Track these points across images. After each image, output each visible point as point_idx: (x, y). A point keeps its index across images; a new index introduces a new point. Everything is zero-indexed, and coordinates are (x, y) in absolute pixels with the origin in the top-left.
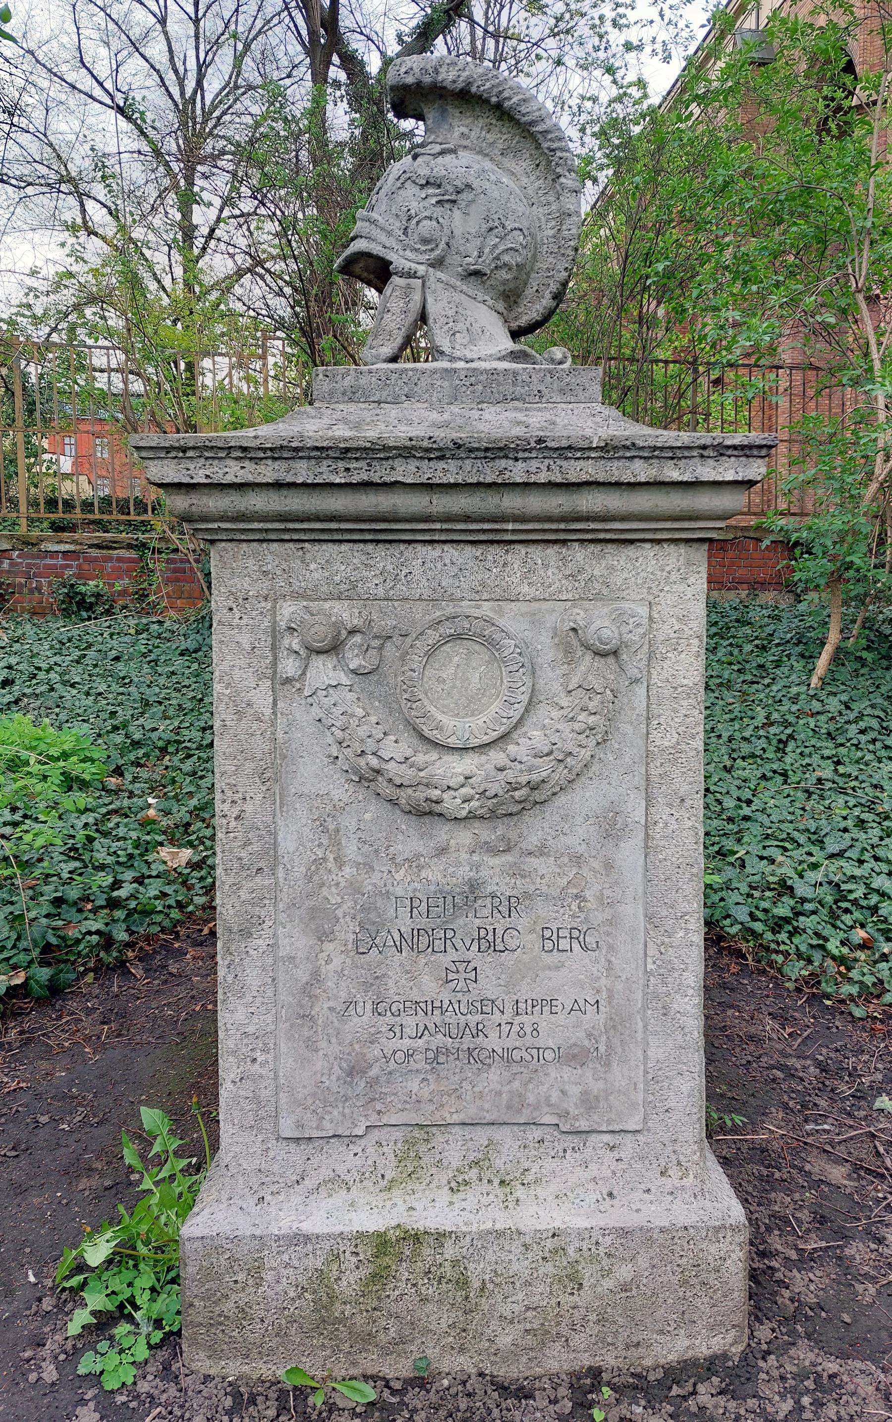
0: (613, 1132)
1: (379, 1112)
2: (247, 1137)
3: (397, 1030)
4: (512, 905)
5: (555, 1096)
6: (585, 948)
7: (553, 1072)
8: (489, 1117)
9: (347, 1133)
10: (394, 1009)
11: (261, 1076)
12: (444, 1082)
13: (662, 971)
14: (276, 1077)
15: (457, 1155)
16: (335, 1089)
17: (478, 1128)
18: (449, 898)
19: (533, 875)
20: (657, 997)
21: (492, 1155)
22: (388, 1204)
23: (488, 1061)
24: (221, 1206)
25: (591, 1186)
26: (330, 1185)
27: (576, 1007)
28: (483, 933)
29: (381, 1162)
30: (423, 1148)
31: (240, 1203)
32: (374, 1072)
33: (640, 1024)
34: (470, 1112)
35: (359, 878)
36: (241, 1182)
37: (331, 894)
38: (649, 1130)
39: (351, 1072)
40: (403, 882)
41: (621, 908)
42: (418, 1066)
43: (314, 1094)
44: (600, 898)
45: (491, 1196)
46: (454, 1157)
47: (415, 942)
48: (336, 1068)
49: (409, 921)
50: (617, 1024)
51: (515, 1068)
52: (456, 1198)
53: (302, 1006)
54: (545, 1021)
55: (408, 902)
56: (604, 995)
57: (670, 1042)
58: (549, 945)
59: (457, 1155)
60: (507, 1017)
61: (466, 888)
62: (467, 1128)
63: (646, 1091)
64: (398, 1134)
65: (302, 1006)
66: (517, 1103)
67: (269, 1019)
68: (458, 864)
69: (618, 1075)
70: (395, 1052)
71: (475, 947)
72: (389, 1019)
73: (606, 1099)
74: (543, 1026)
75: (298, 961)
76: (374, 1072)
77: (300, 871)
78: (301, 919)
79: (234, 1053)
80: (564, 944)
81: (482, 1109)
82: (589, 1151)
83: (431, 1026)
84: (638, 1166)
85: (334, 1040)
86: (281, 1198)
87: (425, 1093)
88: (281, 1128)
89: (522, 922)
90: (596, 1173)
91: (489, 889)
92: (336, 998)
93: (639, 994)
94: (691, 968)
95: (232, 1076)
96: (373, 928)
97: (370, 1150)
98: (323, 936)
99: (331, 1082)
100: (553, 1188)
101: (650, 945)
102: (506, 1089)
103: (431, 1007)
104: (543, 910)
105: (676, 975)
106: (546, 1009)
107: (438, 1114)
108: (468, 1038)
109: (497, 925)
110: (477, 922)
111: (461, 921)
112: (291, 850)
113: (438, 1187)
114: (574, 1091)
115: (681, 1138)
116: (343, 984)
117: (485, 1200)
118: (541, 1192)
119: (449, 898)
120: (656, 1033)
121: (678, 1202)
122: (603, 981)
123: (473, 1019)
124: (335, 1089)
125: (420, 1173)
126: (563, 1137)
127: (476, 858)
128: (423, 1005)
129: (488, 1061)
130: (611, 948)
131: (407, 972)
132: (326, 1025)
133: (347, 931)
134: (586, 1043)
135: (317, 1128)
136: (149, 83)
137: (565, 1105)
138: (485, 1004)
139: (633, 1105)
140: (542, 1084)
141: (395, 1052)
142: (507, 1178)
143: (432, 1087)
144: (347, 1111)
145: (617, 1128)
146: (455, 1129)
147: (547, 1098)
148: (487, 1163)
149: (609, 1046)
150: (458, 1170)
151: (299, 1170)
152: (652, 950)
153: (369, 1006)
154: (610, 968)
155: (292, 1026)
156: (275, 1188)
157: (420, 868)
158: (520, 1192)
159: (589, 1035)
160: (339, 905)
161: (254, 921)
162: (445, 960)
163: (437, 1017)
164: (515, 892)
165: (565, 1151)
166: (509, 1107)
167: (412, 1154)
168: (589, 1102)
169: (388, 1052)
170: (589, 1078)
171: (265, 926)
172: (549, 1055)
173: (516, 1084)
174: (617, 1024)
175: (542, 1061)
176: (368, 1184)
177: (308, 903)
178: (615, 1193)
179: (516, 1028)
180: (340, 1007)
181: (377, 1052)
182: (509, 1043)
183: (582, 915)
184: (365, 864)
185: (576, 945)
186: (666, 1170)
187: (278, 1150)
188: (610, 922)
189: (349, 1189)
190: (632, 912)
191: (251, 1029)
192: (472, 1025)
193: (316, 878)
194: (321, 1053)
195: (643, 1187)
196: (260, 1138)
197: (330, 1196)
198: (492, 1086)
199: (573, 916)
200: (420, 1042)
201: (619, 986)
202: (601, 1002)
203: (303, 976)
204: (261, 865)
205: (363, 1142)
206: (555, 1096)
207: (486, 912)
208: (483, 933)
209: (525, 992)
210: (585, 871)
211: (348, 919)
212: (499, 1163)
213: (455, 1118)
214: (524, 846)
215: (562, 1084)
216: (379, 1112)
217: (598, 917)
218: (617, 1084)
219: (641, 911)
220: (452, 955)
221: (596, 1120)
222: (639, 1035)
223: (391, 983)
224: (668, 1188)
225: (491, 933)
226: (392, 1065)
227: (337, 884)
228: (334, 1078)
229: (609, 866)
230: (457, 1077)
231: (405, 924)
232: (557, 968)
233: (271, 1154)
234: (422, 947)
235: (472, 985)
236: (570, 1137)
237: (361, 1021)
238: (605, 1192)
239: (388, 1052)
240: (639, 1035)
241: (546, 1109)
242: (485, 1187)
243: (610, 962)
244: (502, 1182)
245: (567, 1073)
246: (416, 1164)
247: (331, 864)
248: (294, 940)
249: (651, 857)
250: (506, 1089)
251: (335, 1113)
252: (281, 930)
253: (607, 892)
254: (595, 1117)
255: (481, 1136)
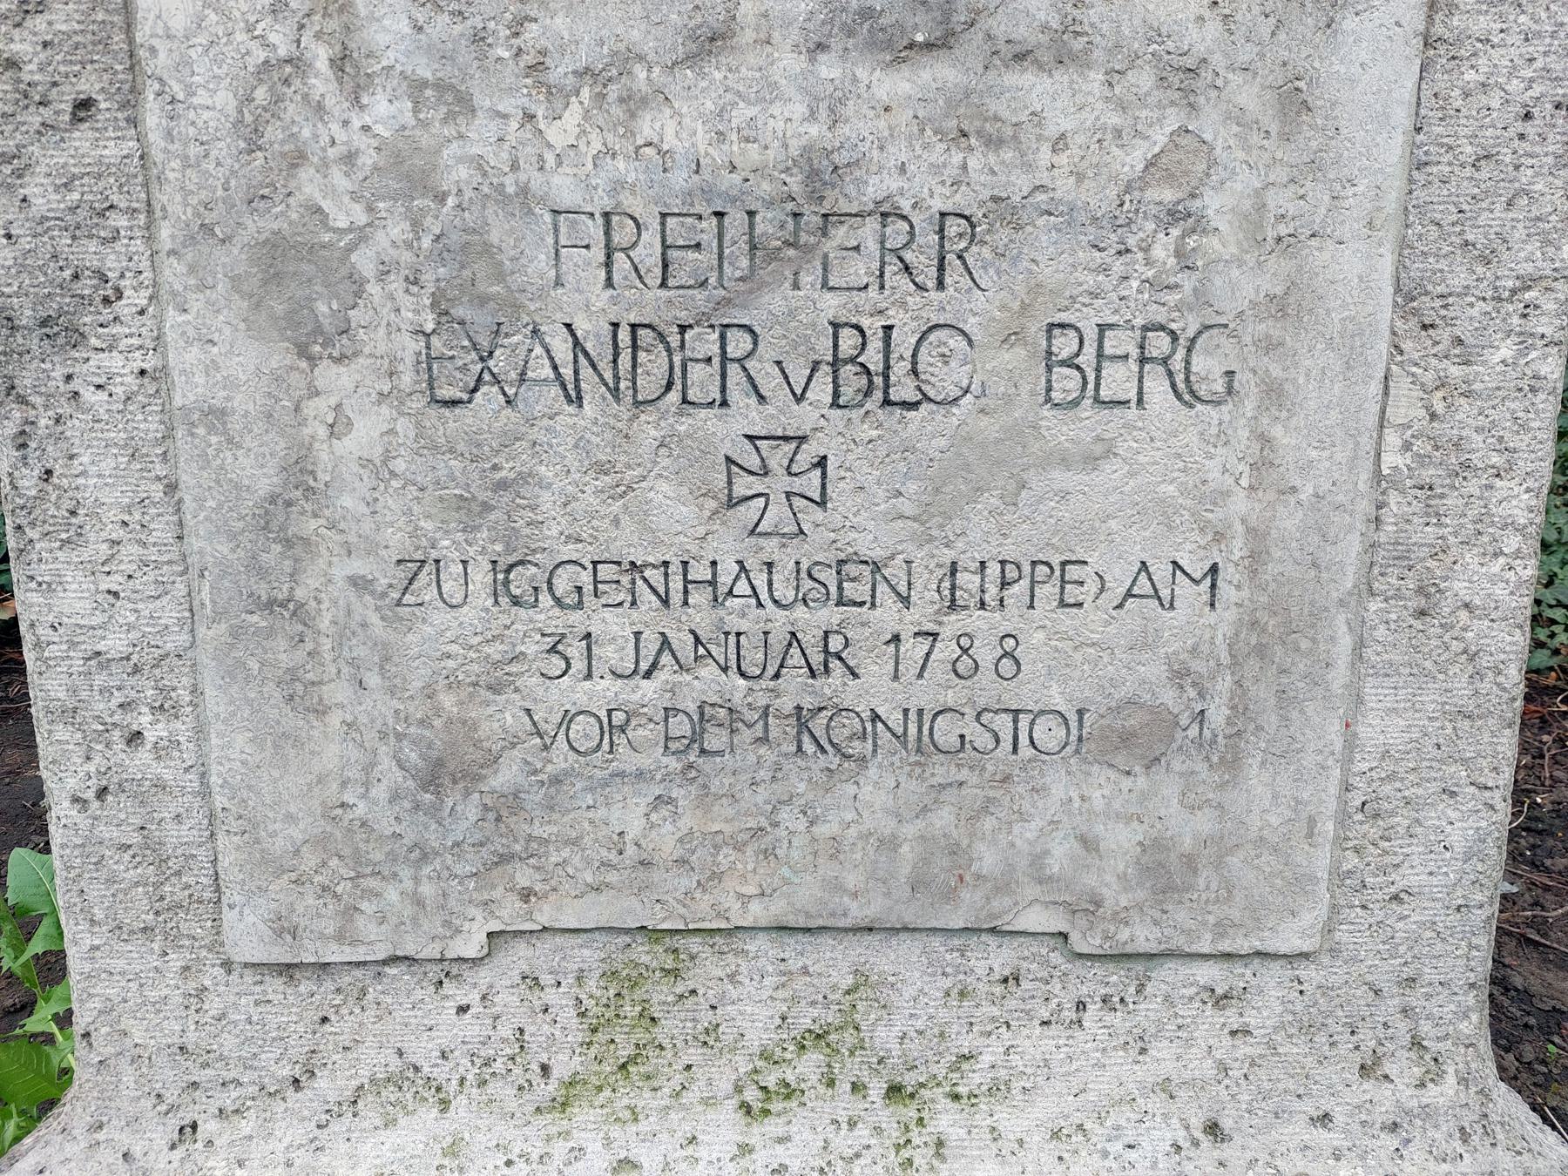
0: (1228, 956)
1: (526, 895)
2: (136, 957)
3: (575, 650)
4: (955, 240)
5: (1061, 853)
6: (1187, 394)
7: (1059, 785)
8: (858, 912)
9: (432, 951)
10: (562, 585)
11: (160, 785)
12: (724, 809)
13: (1428, 474)
14: (205, 792)
15: (763, 1013)
16: (386, 826)
17: (827, 940)
18: (736, 222)
19: (1028, 136)
20: (1404, 558)
21: (866, 1016)
22: (560, 1149)
23: (856, 747)
24: (71, 1149)
25: (1156, 1103)
26: (390, 1093)
27: (1143, 586)
28: (848, 341)
29: (539, 1030)
30: (660, 994)
31: (125, 1139)
32: (506, 776)
33: (1346, 642)
34: (804, 896)
35: (425, 140)
36: (128, 1079)
37: (330, 191)
38: (1334, 952)
39: (434, 776)
40: (574, 158)
41: (1320, 256)
42: (644, 761)
43: (321, 842)
44: (1253, 220)
45: (862, 1131)
46: (754, 1016)
47: (632, 364)
48: (386, 763)
49: (601, 298)
50: (1276, 638)
51: (941, 771)
52: (758, 1133)
53: (263, 573)
54: (1039, 628)
55: (595, 230)
56: (1238, 547)
57: (1430, 699)
58: (1066, 382)
59: (763, 1013)
60: (922, 612)
61: (795, 183)
62: (791, 940)
63: (1340, 842)
64: (588, 955)
65: (263, 573)
66: (945, 870)
67: (170, 612)
68: (769, 93)
69: (1261, 795)
70: (568, 719)
71: (821, 390)
72: (546, 615)
73: (1219, 864)
74: (1034, 642)
75: (235, 424)
76: (506, 776)
77: (215, 104)
78: (236, 281)
79: (70, 714)
80: (1119, 381)
81: (837, 887)
82: (1149, 1010)
83: (682, 642)
84: (1294, 1049)
85: (373, 680)
86: (246, 1126)
87: (666, 841)
88: (228, 935)
89: (978, 305)
90: (1168, 1068)
91: (875, 188)
92: (372, 548)
93: (1352, 547)
94: (1523, 466)
95: (72, 783)
96: (481, 320)
97: (506, 999)
98: (315, 342)
99: (375, 806)
100: (1045, 1109)
101: (1402, 387)
102: (910, 830)
103: (675, 582)
104: (1054, 259)
105: (1473, 487)
106: (1047, 591)
107: (704, 902)
108: (795, 678)
109: (895, 317)
110: (831, 305)
111: (776, 300)
112: (178, 24)
113: (707, 1102)
114: (1121, 839)
115: (1429, 974)
116: (391, 503)
117: (844, 1142)
118: (1011, 1122)
119: (736, 222)
120: (1389, 671)
121: (1415, 1152)
122: (1240, 504)
123: (813, 620)
124: (386, 826)
125: (655, 1060)
126: (1079, 968)
127: (829, 69)
128: (655, 576)
129: (856, 747)
130: (1274, 393)
131: (602, 469)
132: (342, 636)
133: (393, 323)
134: (1168, 697)
135: (340, 937)
136: (893, 918)
137: (1090, 880)
138: (847, 577)
139: (1301, 883)
140: (1023, 817)
141: (568, 719)
142: (910, 1080)
143: (686, 822)
144: (427, 889)
145: (1244, 945)
146: (757, 944)
147: (1038, 859)
148: (849, 1037)
149: (1240, 708)
150: (765, 1055)
151: (298, 1050)
152: (1406, 406)
153: (481, 576)
154: (1263, 464)
155: (236, 633)
156: (228, 1098)
157: (634, 104)
158: (947, 1120)
159: (1179, 675)
160: (361, 235)
161: (86, 286)
162: (725, 431)
163: (700, 614)
164: (961, 200)
165: (1081, 1006)
166: (916, 885)
167: (630, 1011)
168: (1164, 873)
169: (548, 718)
170: (1171, 805)
171: (124, 308)
172: (1049, 734)
173: (943, 818)
174: (1276, 638)
175: (1026, 751)
176: (502, 1090)
177: (256, 226)
178: (1227, 1123)
179: (946, 650)
180: (387, 576)
181: (512, 719)
182: (924, 696)
183: (1188, 282)
184: (441, 86)
185: (1157, 386)
186: (1377, 1059)
187: (231, 997)
188: (1279, 306)
189: (445, 1104)
190: (1356, 272)
191: (114, 644)
192: (810, 639)
193: (273, 133)
194: (335, 719)
195: (1309, 1107)
196: (176, 961)
197: (389, 1123)
198: (868, 824)
199: (1157, 285)
200: (649, 688)
201: (1289, 521)
202: (1228, 573)
203: (257, 472)
204: (88, 85)
205: (484, 976)
206: (1061, 853)
207: (860, 270)
208: (848, 341)
209: (980, 536)
210: (1210, 124)
211: (396, 284)
212: (885, 1037)
213: (757, 913)
214: (1000, 26)
215: (1085, 819)
216: (526, 895)
217: (1241, 286)
218: (1255, 821)
219: (1387, 265)
220: (747, 416)
221: (1183, 923)
222: (1339, 676)
223: (548, 502)
224: (1384, 1111)
225: (875, 344)
226: (561, 758)
227: (350, 158)
228: (380, 792)
229: (1294, 100)
230: (763, 793)
231: (590, 305)
232: (1091, 461)
233: (213, 1005)
234: (649, 386)
235: (811, 516)
236: (1098, 969)
237: (458, 620)
238: (1197, 1123)
239: (548, 718)
240: (1339, 676)
241: (1031, 891)
242: (843, 1104)
243: (1265, 440)
244: (894, 1091)
245: (1102, 787)
246: (640, 1036)
247: (322, 83)
248: (216, 350)
249: (1440, 80)
250: (910, 830)
251: (392, 894)
252: (172, 316)
253: (1279, 200)
254: (1181, 916)
255: (834, 963)
